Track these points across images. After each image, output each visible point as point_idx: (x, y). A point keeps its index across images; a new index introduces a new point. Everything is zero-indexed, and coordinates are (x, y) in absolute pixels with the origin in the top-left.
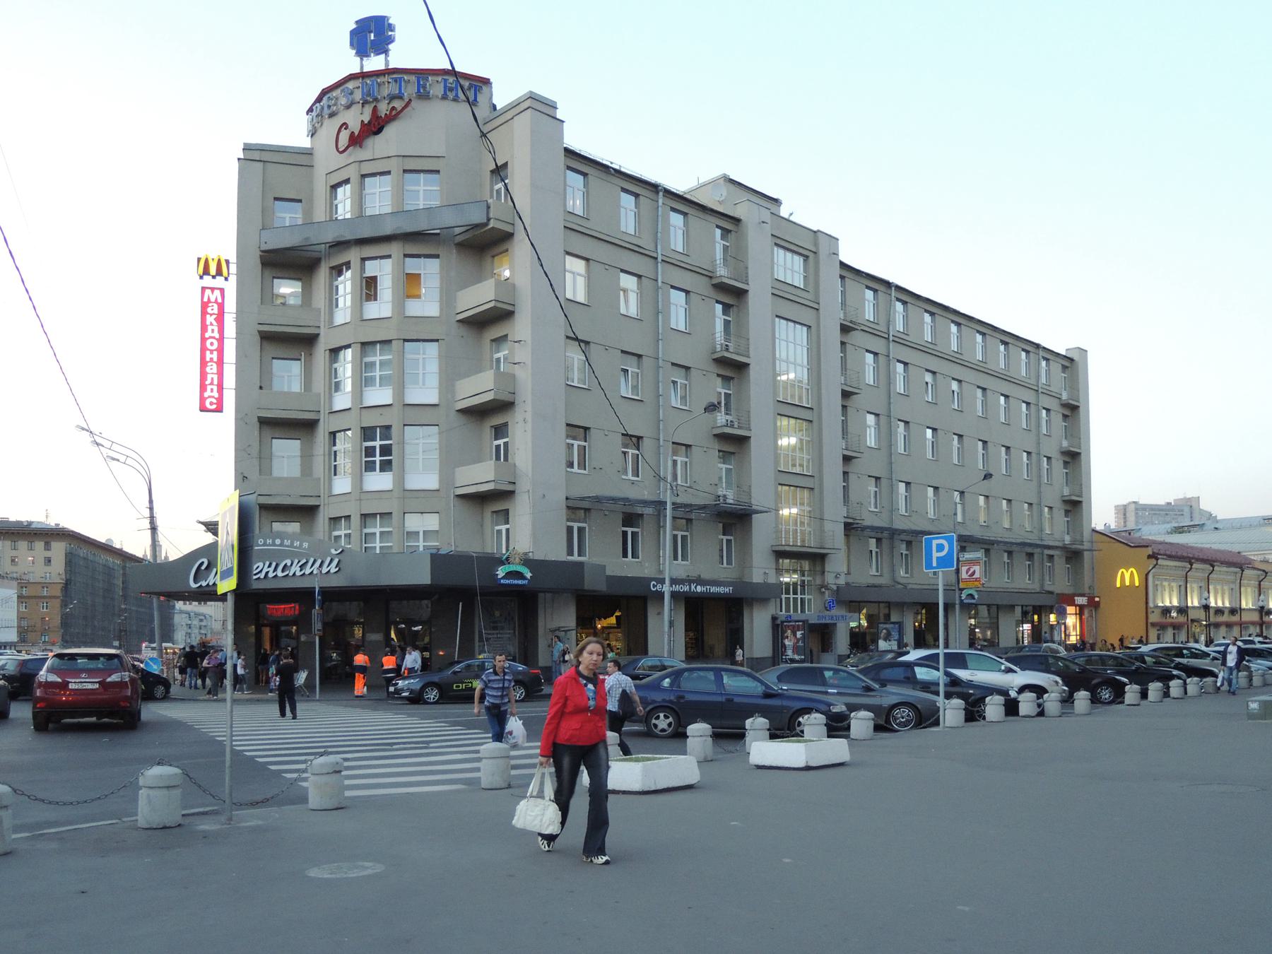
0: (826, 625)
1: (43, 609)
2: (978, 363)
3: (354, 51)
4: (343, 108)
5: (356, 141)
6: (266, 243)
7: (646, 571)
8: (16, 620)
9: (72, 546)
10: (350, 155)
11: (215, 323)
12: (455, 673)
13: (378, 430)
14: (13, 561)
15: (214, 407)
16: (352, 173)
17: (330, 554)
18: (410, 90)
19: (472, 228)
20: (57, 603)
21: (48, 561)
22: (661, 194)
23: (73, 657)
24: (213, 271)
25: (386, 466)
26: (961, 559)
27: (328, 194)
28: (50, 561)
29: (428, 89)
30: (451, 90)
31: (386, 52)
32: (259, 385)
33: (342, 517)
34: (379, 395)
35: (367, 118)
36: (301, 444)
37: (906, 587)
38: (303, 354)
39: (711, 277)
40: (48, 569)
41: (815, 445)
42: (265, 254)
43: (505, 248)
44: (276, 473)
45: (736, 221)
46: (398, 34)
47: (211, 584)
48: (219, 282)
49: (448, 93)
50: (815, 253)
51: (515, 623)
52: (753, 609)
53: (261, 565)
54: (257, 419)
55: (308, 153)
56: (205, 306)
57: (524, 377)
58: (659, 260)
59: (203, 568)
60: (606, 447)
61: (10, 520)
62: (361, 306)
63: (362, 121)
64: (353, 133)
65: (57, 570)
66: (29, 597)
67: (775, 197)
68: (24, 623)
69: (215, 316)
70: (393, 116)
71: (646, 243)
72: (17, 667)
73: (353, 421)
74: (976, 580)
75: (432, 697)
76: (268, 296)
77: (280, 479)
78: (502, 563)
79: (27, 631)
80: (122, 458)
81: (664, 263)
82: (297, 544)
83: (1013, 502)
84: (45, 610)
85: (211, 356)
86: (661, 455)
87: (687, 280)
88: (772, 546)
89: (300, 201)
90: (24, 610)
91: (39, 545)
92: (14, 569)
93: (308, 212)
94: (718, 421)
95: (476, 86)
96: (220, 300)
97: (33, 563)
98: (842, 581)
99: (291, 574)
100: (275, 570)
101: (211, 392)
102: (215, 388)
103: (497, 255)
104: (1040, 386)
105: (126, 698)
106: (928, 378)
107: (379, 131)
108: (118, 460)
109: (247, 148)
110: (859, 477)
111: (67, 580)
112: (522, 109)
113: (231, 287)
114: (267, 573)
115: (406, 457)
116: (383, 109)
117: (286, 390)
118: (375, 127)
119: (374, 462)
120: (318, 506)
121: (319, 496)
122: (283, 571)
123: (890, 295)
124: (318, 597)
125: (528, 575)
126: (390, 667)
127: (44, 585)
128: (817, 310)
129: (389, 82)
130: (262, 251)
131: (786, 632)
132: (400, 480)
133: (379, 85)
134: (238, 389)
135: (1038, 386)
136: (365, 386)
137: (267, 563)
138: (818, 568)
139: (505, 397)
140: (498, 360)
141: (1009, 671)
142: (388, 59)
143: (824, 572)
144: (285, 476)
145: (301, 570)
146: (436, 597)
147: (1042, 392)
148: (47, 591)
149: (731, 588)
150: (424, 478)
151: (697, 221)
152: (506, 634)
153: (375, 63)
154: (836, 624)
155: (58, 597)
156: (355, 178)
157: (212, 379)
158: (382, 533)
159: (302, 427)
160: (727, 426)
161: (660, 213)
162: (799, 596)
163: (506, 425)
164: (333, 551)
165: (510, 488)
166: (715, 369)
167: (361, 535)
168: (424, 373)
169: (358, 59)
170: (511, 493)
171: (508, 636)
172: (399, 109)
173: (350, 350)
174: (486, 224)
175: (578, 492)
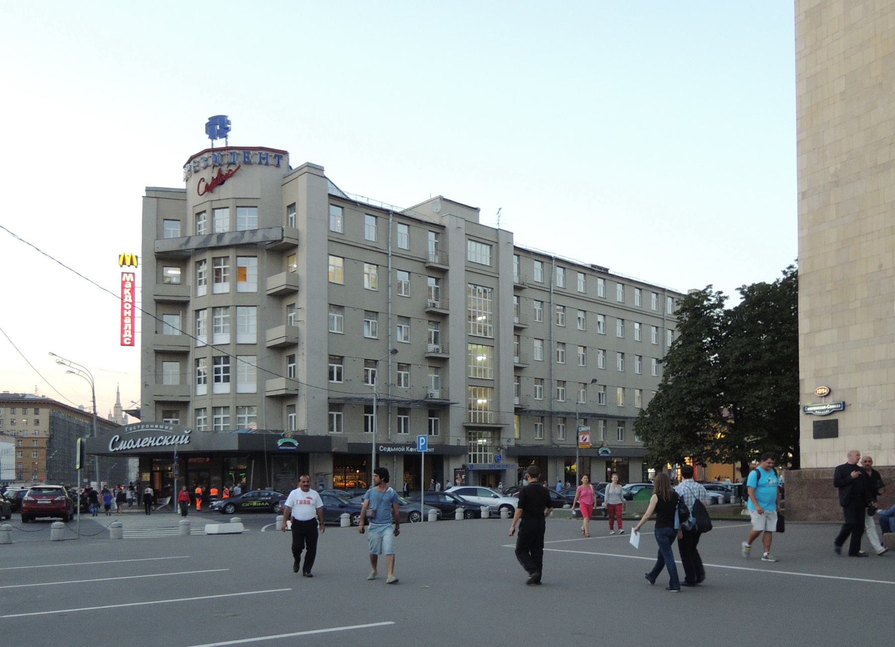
0: (499, 471)
1: (34, 456)
2: (619, 304)
3: (208, 136)
4: (202, 168)
5: (209, 188)
6: (158, 248)
7: (380, 439)
8: (14, 465)
9: (54, 411)
10: (206, 196)
11: (129, 293)
12: (244, 498)
13: (222, 358)
14: (12, 422)
15: (129, 343)
16: (207, 207)
17: (184, 433)
18: (240, 160)
19: (271, 243)
20: (44, 452)
21: (37, 422)
22: (391, 215)
23: (40, 489)
24: (128, 262)
25: (227, 379)
26: (579, 431)
27: (194, 219)
28: (38, 422)
29: (250, 158)
30: (264, 159)
31: (226, 137)
32: (155, 331)
33: (202, 408)
34: (222, 338)
35: (215, 176)
36: (180, 364)
37: (558, 447)
38: (181, 312)
39: (425, 263)
40: (37, 428)
41: (496, 360)
42: (158, 254)
43: (293, 252)
44: (165, 383)
45: (443, 227)
46: (233, 126)
47: (121, 449)
48: (132, 269)
49: (262, 161)
50: (497, 243)
51: (296, 470)
52: (449, 461)
53: (147, 439)
54: (153, 351)
55: (183, 192)
56: (123, 283)
57: (303, 328)
58: (390, 255)
59: (117, 440)
60: (353, 369)
61: (10, 393)
62: (213, 286)
63: (213, 177)
64: (207, 184)
65: (44, 428)
66: (24, 448)
67: (475, 207)
68: (20, 466)
69: (129, 290)
70: (230, 175)
71: (382, 246)
72: (15, 495)
73: (209, 353)
74: (587, 443)
75: (231, 510)
76: (160, 278)
77: (166, 386)
78: (281, 438)
79: (22, 472)
80: (77, 372)
81: (394, 257)
82: (161, 427)
83: (643, 391)
84: (35, 457)
85: (128, 313)
86: (390, 371)
87: (410, 266)
88: (463, 423)
89: (179, 220)
90: (20, 457)
91: (31, 411)
92: (13, 428)
93: (184, 229)
94: (429, 349)
95: (279, 156)
96: (132, 280)
97: (26, 424)
98: (512, 443)
99: (164, 444)
100: (155, 442)
101: (128, 334)
102: (130, 332)
103: (291, 256)
104: (665, 315)
105: (63, 508)
106: (581, 315)
107: (222, 183)
108: (74, 373)
109: (148, 190)
110: (528, 379)
111: (50, 435)
112: (303, 172)
113: (138, 272)
114: (151, 443)
115: (238, 373)
116: (225, 170)
117: (171, 334)
118: (220, 180)
119: (220, 377)
120: (189, 402)
121: (189, 396)
122: (159, 442)
123: (552, 264)
124: (176, 457)
125: (297, 444)
126: (214, 494)
127: (34, 439)
128: (498, 278)
129: (228, 155)
130: (156, 253)
131: (457, 475)
132: (234, 387)
133: (222, 156)
134: (143, 332)
135: (664, 316)
136: (215, 333)
137: (151, 438)
138: (496, 436)
139: (292, 340)
140: (291, 317)
141: (496, 497)
142: (227, 140)
143: (499, 439)
144: (171, 384)
145: (169, 442)
146: (249, 455)
147: (666, 319)
148: (36, 443)
149: (433, 449)
150: (248, 385)
151: (417, 230)
152: (291, 476)
153: (220, 143)
154: (505, 470)
155: (43, 448)
156: (209, 211)
157: (128, 327)
158: (224, 418)
159: (181, 355)
160: (434, 352)
161: (390, 227)
162: (483, 453)
163: (294, 355)
164: (186, 432)
165: (295, 393)
166: (427, 318)
167: (212, 419)
168: (248, 326)
169: (210, 140)
170: (296, 395)
171: (292, 477)
172: (234, 170)
173: (205, 311)
174: (281, 240)
175: (334, 395)
